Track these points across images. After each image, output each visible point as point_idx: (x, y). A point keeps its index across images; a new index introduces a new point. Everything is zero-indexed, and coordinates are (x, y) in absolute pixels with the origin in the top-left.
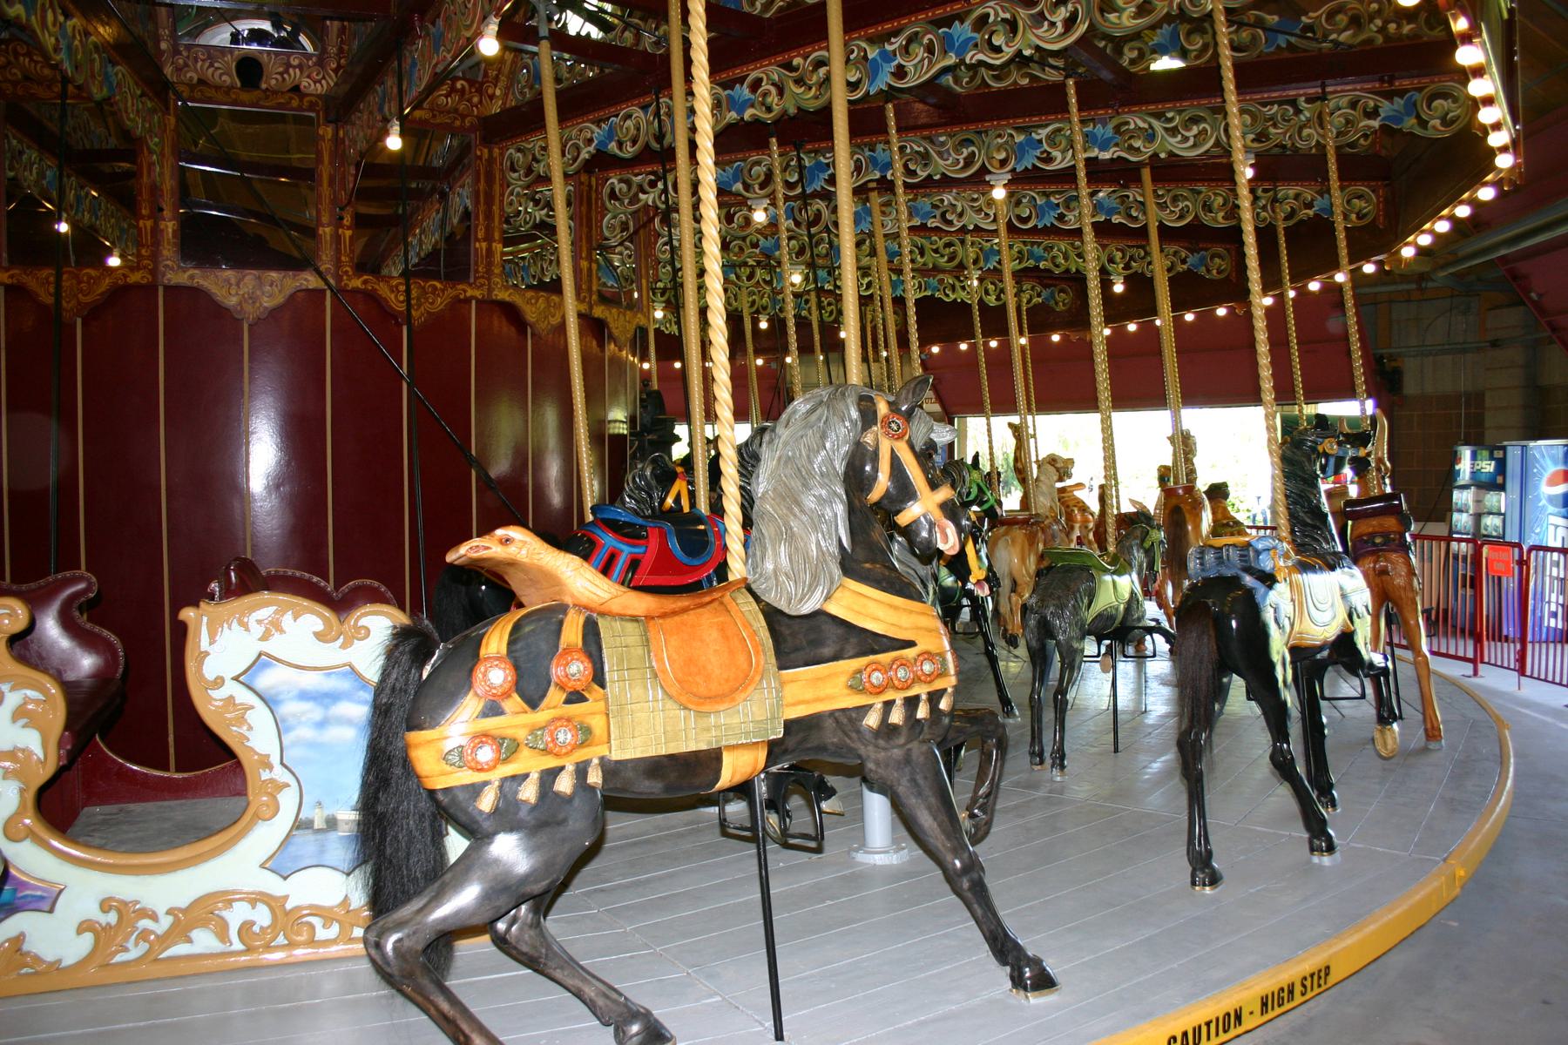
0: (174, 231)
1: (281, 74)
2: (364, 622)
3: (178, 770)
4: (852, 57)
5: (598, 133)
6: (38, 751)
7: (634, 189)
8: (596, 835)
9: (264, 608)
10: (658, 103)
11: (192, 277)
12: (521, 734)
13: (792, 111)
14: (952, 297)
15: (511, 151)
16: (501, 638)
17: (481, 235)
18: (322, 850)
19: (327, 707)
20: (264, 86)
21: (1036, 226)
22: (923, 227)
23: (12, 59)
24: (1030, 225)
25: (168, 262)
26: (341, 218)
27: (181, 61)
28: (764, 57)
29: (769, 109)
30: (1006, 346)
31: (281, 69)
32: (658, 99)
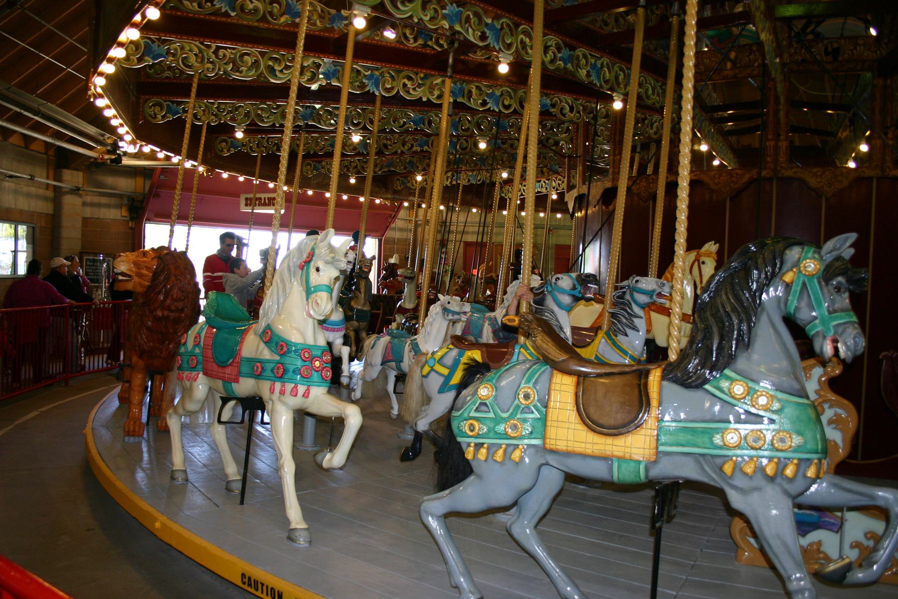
0: (786, 147)
1: (851, 50)
3: (862, 459)
6: (839, 441)
25: (783, 165)
27: (793, 51)
31: (852, 48)
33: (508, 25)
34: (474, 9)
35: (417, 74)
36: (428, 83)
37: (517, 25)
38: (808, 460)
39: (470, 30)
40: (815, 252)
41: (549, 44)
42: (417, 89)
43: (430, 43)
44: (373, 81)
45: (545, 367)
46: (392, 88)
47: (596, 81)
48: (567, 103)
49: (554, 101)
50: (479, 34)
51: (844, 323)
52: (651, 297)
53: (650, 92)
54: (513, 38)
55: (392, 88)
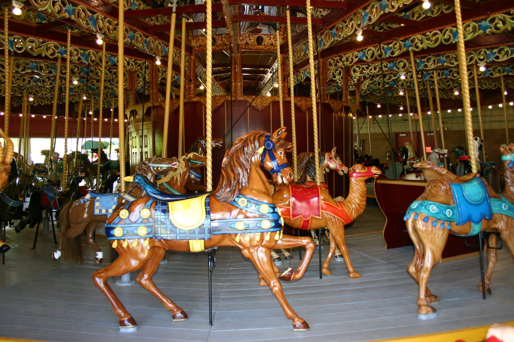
5: (360, 55)
7: (336, 61)
8: (458, 232)
10: (380, 46)
11: (244, 98)
13: (425, 48)
15: (330, 60)
21: (483, 77)
22: (507, 75)
24: (482, 76)
28: (416, 33)
29: (417, 47)
30: (98, 121)
32: (380, 45)
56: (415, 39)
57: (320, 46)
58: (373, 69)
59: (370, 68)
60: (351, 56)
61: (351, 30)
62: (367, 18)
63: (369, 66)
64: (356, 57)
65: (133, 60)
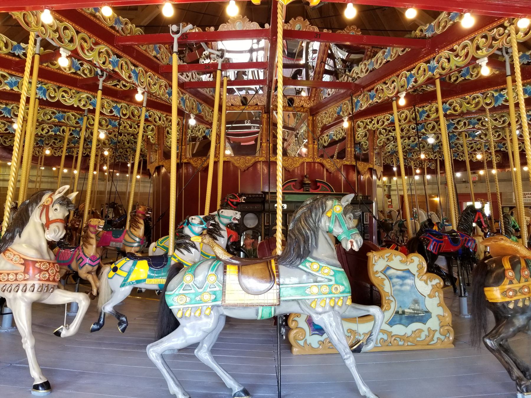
1: (299, 102)
2: (414, 258)
4: (488, 96)
7: (388, 131)
9: (388, 252)
12: (517, 289)
14: (462, 159)
16: (508, 263)
17: (349, 146)
18: (401, 319)
19: (403, 281)
20: (294, 106)
23: (229, 100)
26: (314, 142)
33: (142, 71)
34: (126, 60)
35: (71, 90)
36: (78, 96)
37: (146, 72)
38: (347, 296)
39: (123, 72)
40: (338, 202)
41: (162, 84)
42: (71, 99)
43: (78, 72)
44: (42, 91)
45: (220, 262)
46: (55, 97)
47: (183, 107)
48: (157, 115)
49: (150, 114)
50: (128, 75)
51: (354, 234)
52: (230, 220)
53: (207, 115)
54: (145, 79)
55: (55, 97)
56: (454, 102)
57: (356, 108)
58: (376, 123)
59: (373, 122)
60: (408, 127)
61: (463, 61)
62: (413, 79)
63: (372, 120)
64: (388, 120)
65: (165, 115)
